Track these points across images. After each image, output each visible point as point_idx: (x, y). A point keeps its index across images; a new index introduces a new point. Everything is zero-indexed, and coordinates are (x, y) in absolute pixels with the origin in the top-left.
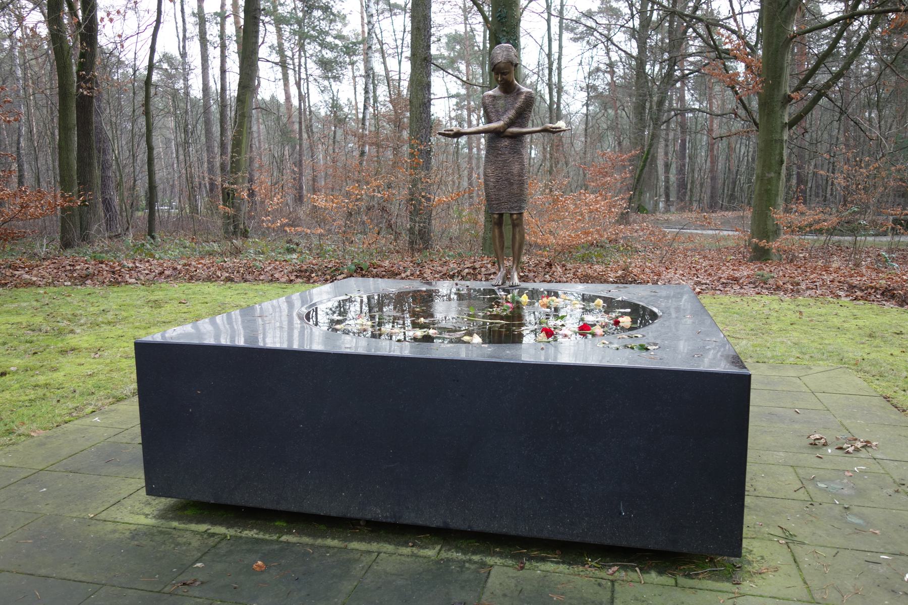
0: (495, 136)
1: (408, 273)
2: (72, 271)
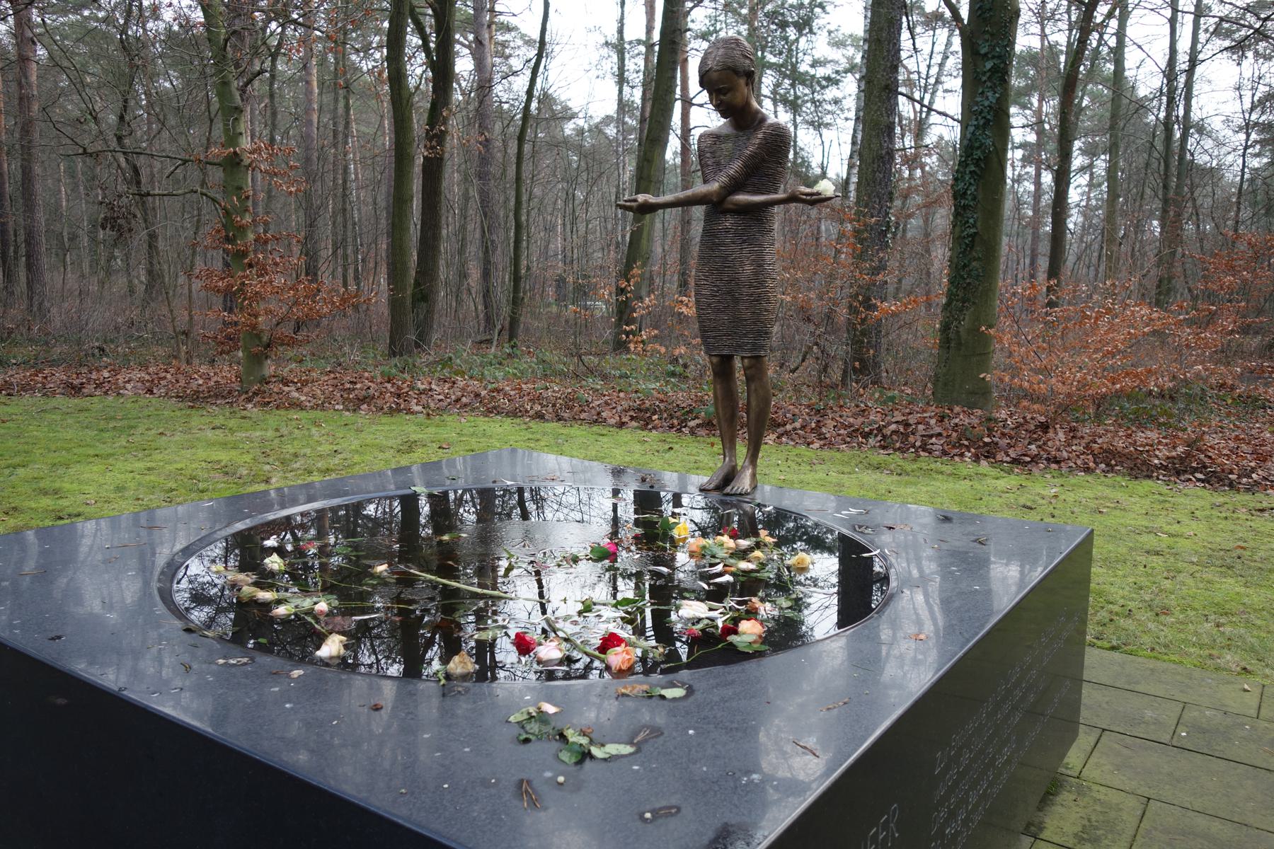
0: (716, 205)
1: (797, 425)
2: (350, 391)
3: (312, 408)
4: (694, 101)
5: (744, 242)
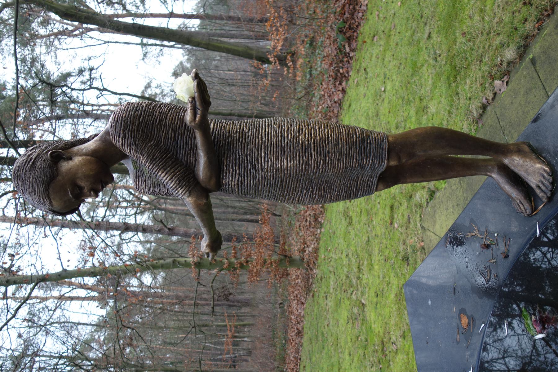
3: (318, 244)
4: (171, 11)
5: (254, 167)
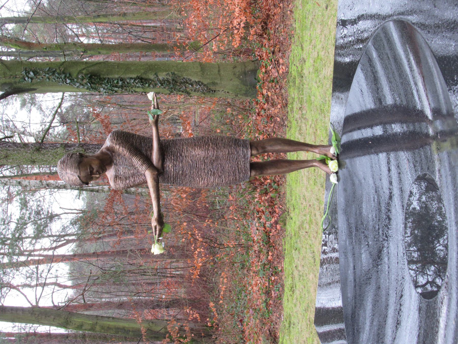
5: (181, 155)
